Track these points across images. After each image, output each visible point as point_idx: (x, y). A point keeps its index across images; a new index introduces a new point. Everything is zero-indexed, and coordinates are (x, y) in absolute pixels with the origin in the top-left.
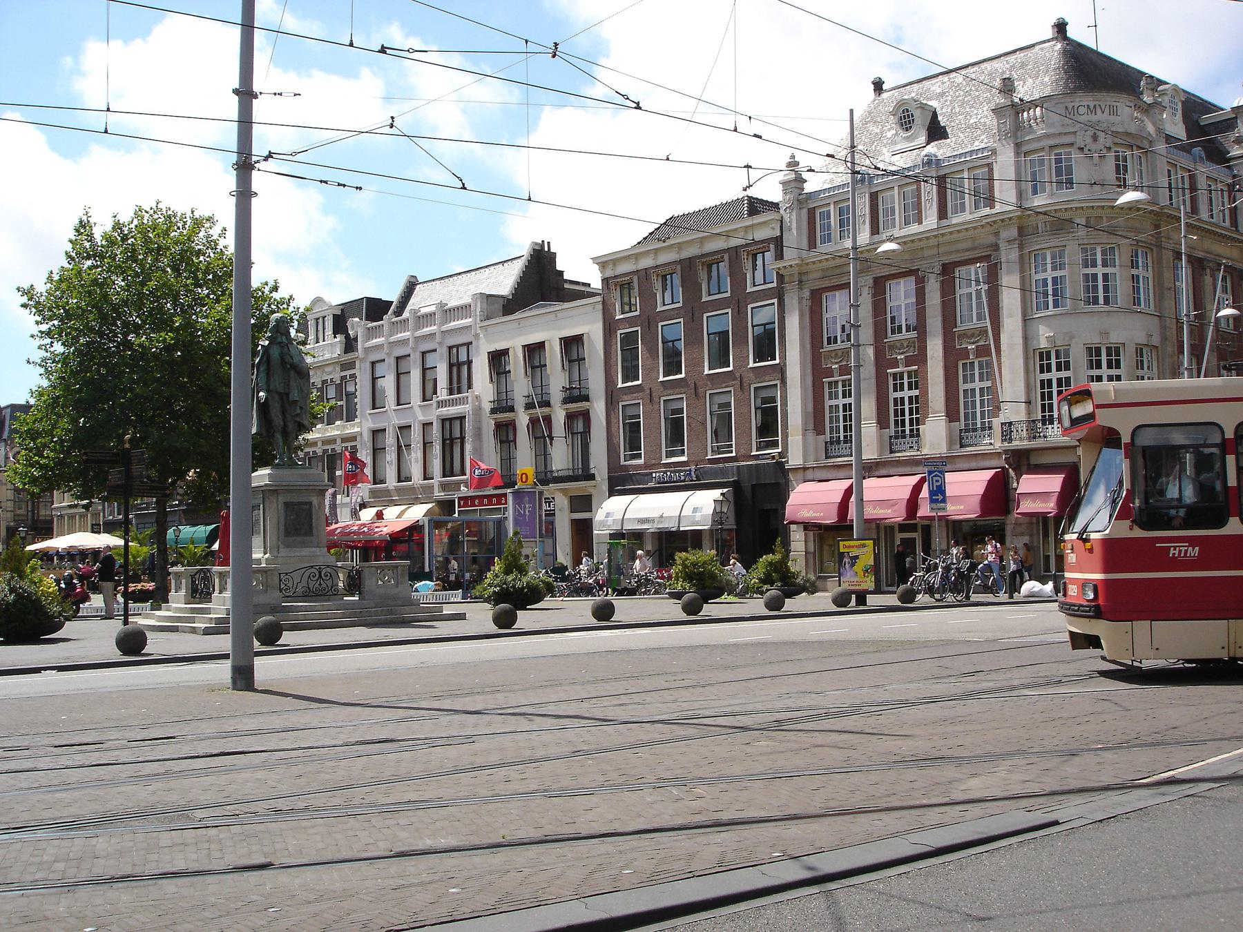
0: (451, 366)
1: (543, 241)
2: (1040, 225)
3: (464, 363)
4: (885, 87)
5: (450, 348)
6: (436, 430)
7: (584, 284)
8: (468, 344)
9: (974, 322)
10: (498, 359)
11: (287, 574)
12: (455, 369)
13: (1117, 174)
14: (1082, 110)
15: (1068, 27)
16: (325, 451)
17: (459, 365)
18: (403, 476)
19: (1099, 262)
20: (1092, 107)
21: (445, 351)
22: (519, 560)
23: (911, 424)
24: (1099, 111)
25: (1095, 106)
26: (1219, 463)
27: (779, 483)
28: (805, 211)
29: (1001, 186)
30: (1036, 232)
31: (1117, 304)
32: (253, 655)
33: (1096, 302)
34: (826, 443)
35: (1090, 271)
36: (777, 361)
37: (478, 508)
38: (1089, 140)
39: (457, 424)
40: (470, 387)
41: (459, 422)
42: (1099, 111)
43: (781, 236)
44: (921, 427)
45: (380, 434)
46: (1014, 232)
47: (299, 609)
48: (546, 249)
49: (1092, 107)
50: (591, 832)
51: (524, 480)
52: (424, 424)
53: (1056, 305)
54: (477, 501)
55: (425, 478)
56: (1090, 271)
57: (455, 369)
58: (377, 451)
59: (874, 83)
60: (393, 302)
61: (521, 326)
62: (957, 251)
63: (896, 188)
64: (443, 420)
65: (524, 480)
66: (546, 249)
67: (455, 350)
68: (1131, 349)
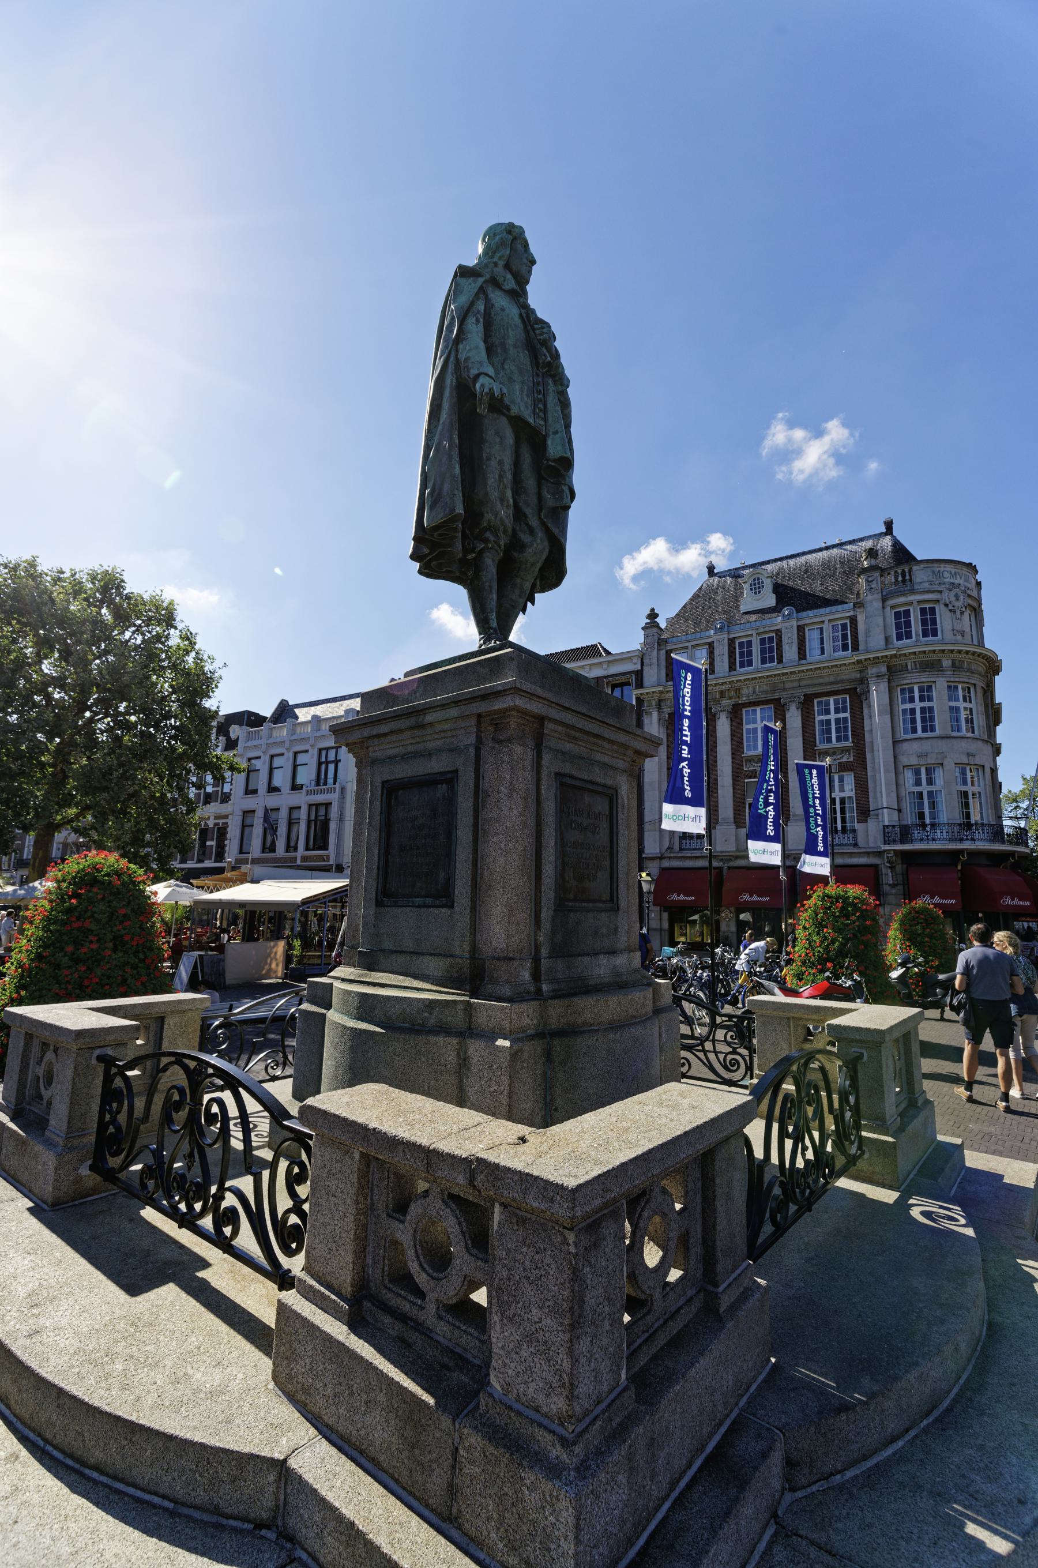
2: (909, 664)
3: (331, 762)
5: (320, 750)
6: (303, 814)
9: (938, 732)
16: (216, 824)
17: (327, 763)
18: (244, 850)
21: (316, 752)
30: (904, 668)
31: (450, 778)
35: (926, 704)
38: (953, 599)
43: (642, 670)
45: (250, 814)
46: (883, 669)
52: (244, 812)
53: (924, 730)
55: (241, 852)
56: (926, 704)
58: (291, 823)
59: (885, 523)
62: (820, 684)
63: (827, 622)
64: (310, 806)
67: (324, 753)
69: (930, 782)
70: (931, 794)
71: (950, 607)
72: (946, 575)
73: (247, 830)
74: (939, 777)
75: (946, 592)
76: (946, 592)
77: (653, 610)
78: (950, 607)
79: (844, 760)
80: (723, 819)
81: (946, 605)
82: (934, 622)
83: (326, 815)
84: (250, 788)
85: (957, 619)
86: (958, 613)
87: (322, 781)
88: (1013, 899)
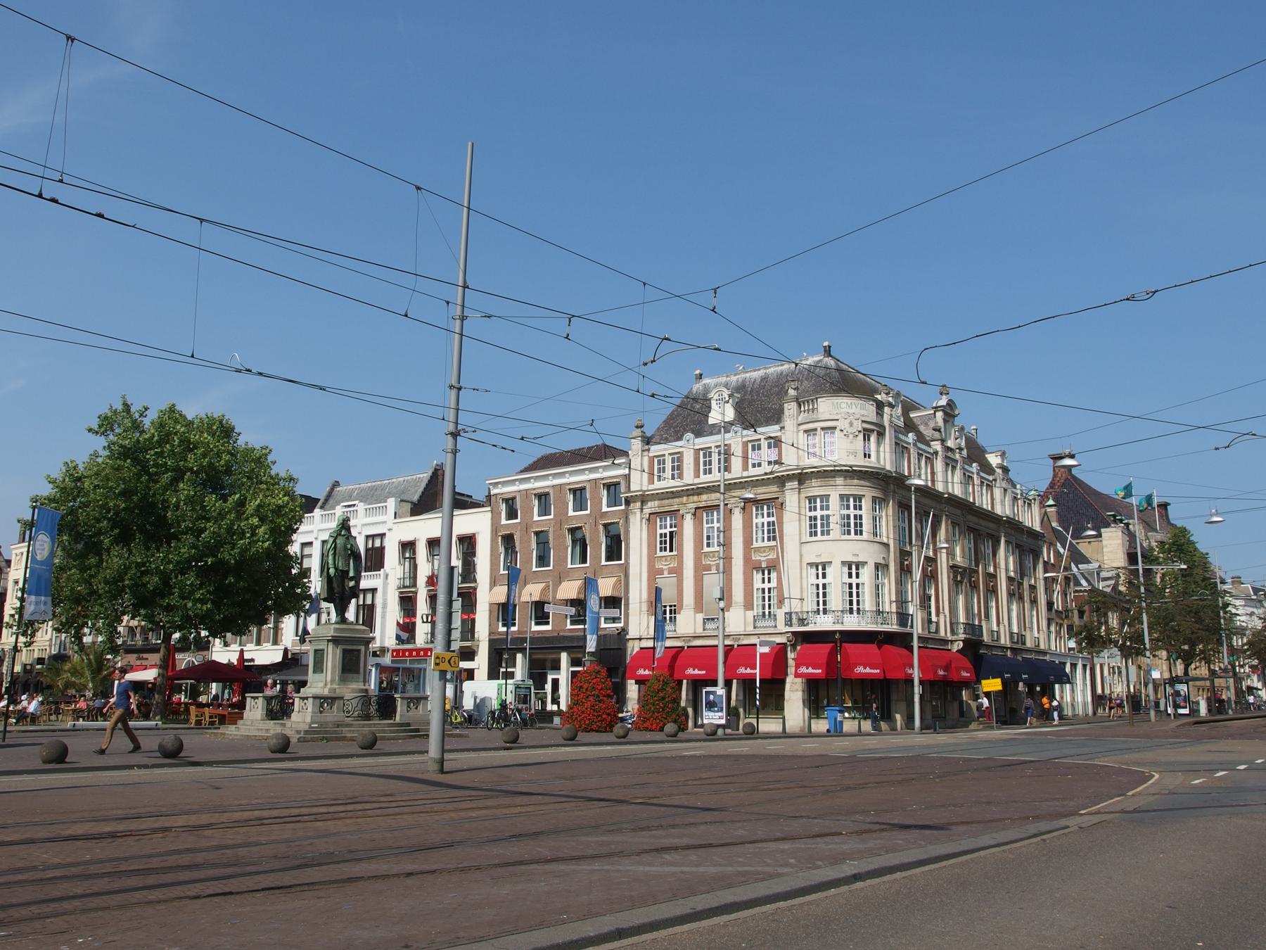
7: (468, 496)
8: (382, 536)
10: (408, 547)
11: (348, 700)
14: (843, 405)
19: (818, 507)
20: (849, 403)
23: (671, 613)
24: (854, 406)
25: (851, 403)
26: (627, 662)
27: (620, 649)
28: (646, 459)
33: (849, 533)
34: (754, 617)
36: (623, 562)
37: (408, 659)
38: (847, 425)
41: (371, 595)
42: (854, 406)
44: (677, 616)
47: (386, 726)
49: (849, 403)
50: (600, 932)
53: (823, 534)
54: (407, 654)
60: (319, 500)
71: (845, 433)
78: (845, 433)
79: (672, 566)
81: (842, 431)
88: (807, 668)
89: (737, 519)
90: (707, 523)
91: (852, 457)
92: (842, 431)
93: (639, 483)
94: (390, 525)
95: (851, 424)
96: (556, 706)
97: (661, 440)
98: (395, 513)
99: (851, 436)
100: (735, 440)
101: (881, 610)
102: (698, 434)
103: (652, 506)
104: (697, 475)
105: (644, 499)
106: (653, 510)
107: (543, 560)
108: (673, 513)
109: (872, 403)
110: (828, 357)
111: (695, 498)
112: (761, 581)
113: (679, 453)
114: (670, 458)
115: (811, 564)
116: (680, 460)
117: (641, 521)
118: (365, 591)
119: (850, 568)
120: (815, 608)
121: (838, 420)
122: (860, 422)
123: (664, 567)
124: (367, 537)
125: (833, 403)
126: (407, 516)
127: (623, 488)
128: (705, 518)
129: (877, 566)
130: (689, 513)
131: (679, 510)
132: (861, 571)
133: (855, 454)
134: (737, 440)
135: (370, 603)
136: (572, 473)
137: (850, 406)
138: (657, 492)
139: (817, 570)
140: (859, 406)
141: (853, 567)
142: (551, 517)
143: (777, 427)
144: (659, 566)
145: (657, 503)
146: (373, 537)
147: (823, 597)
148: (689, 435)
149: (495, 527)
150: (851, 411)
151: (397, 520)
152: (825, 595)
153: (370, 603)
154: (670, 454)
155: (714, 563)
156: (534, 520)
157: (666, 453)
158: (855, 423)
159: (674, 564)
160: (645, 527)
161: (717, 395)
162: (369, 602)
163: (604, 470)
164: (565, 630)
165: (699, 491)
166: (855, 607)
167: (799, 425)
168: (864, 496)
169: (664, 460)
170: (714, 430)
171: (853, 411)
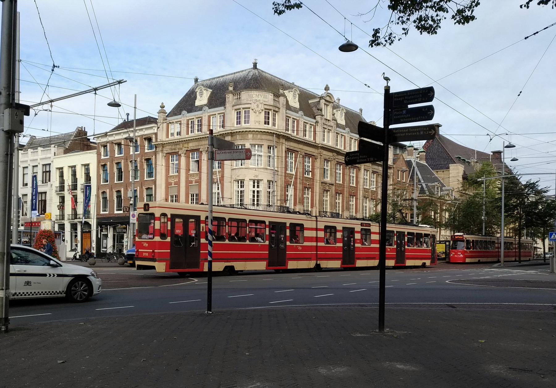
0: (43, 172)
1: (82, 127)
3: (48, 172)
4: (198, 80)
8: (50, 164)
12: (44, 174)
13: (265, 119)
15: (257, 64)
20: (257, 95)
22: (525, 202)
24: (260, 96)
25: (259, 95)
29: (283, 128)
32: (9, 274)
36: (154, 179)
38: (255, 107)
39: (44, 195)
40: (49, 181)
42: (260, 96)
48: (83, 130)
49: (257, 95)
51: (47, 217)
57: (44, 174)
61: (243, 167)
65: (47, 217)
66: (83, 130)
68: (265, 181)
69: (258, 187)
70: (258, 192)
71: (254, 111)
72: (254, 96)
73: (25, 176)
74: (261, 184)
75: (253, 104)
76: (253, 104)
77: (162, 104)
78: (254, 111)
79: (176, 181)
80: (181, 201)
81: (253, 110)
82: (249, 117)
83: (212, 164)
84: (25, 183)
85: (257, 116)
86: (257, 113)
87: (44, 181)
89: (183, 160)
90: (192, 158)
91: (257, 124)
92: (253, 110)
93: (162, 137)
94: (52, 159)
95: (258, 106)
96: (318, 263)
97: (173, 114)
98: (55, 153)
99: (257, 113)
100: (204, 114)
101: (271, 204)
102: (189, 111)
103: (167, 149)
104: (188, 134)
105: (163, 145)
106: (168, 152)
107: (120, 178)
108: (197, 150)
109: (271, 94)
110: (255, 69)
111: (186, 145)
112: (252, 186)
113: (223, 113)
114: (243, 111)
115: (235, 180)
116: (201, 121)
117: (162, 158)
118: (42, 193)
119: (254, 183)
120: (237, 203)
121: (251, 104)
122: (263, 105)
123: (172, 181)
124: (43, 165)
125: (249, 95)
126: (61, 155)
127: (154, 140)
128: (191, 156)
129: (269, 182)
130: (183, 153)
131: (200, 149)
132: (260, 184)
133: (259, 122)
134: (205, 114)
135: (44, 199)
136: (146, 129)
137: (258, 96)
138: (200, 137)
139: (238, 183)
140: (263, 96)
141: (256, 182)
142: (123, 155)
143: (223, 108)
144: (170, 181)
145: (170, 147)
146: (46, 165)
147: (257, 198)
148: (184, 112)
149: (99, 160)
150: (258, 99)
151: (55, 157)
152: (258, 196)
153: (44, 199)
154: (219, 114)
155: (194, 179)
156: (115, 156)
157: (217, 113)
158: (260, 106)
159: (177, 180)
160: (164, 161)
161: (199, 90)
162: (43, 199)
163: (146, 130)
164: (113, 214)
165: (187, 141)
166: (256, 203)
167: (233, 106)
168: (263, 145)
169: (240, 112)
170: (200, 108)
171: (259, 99)
